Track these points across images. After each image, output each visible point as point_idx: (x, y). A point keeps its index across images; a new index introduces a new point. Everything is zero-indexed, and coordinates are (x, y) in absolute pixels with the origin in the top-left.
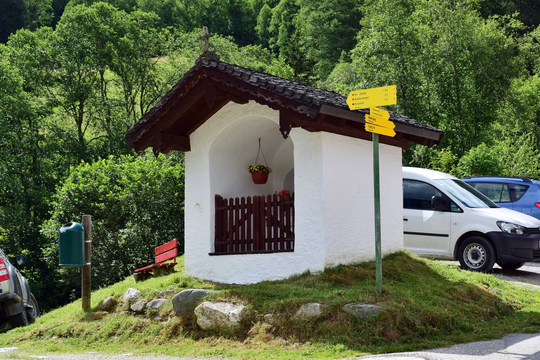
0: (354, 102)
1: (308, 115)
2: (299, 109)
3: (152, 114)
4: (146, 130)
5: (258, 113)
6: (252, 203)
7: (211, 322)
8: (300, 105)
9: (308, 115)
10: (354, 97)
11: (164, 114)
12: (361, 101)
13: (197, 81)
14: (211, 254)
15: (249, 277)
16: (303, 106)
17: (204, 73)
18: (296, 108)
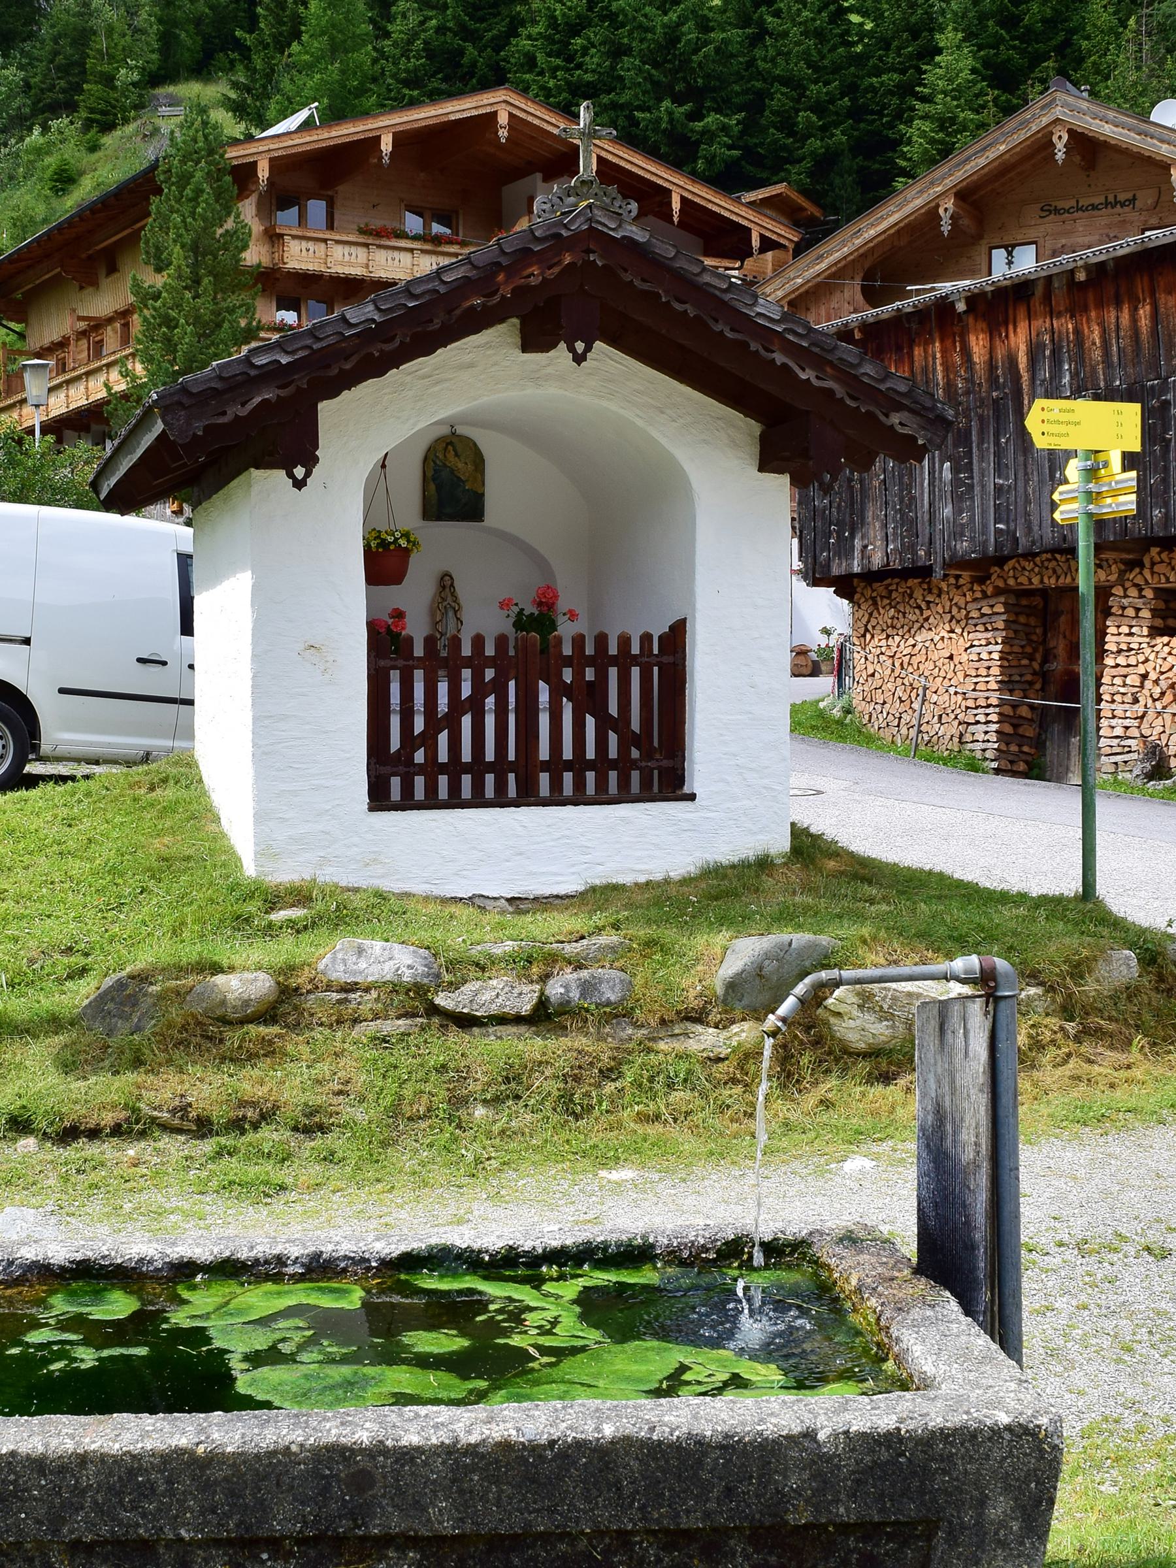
0: (1046, 428)
1: (920, 442)
2: (895, 419)
3: (319, 339)
4: (283, 393)
5: (583, 390)
6: (512, 653)
7: (893, 1027)
8: (899, 407)
9: (920, 442)
10: (1045, 415)
11: (381, 351)
12: (1062, 429)
13: (556, 270)
14: (793, 825)
15: (531, 874)
16: (906, 414)
17: (594, 252)
18: (887, 416)
